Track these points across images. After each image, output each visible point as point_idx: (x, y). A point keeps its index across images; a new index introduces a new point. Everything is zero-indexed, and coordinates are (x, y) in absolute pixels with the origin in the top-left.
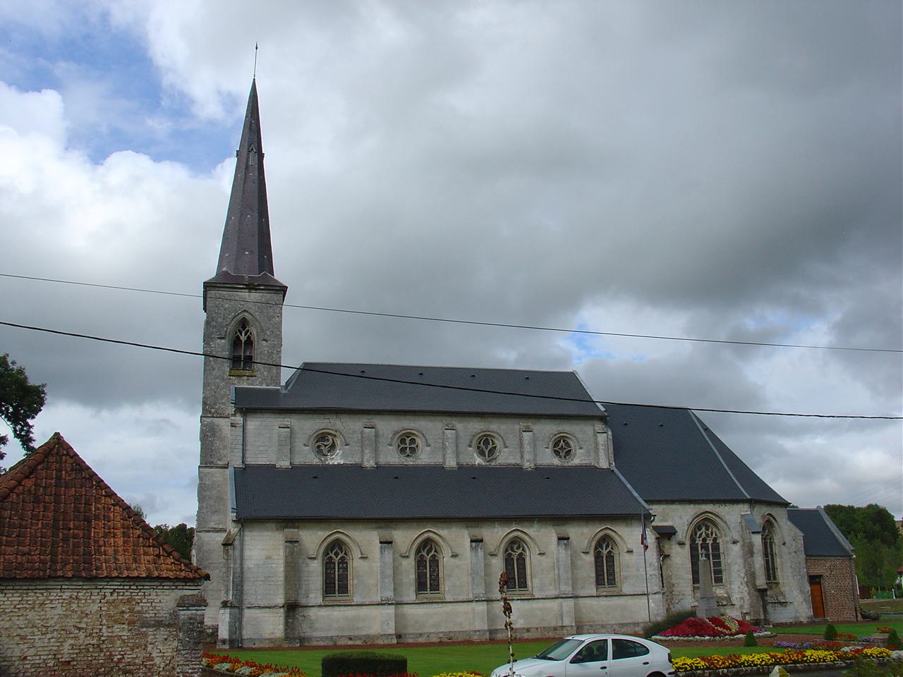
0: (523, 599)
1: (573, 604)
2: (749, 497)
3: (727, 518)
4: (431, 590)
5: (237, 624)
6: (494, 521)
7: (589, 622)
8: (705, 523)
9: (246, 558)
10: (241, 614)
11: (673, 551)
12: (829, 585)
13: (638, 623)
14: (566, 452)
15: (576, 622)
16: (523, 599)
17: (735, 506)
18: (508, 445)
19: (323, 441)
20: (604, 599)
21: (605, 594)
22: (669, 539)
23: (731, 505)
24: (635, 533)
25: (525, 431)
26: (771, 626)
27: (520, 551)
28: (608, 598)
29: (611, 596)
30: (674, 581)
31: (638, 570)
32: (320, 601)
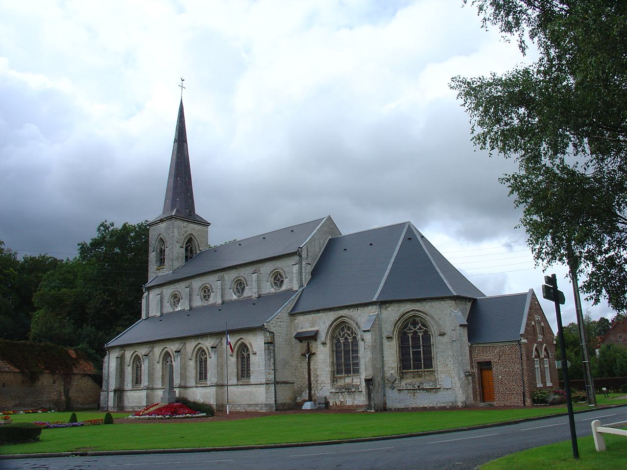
0: (203, 387)
1: (145, 393)
2: (455, 294)
3: (359, 320)
4: (424, 368)
5: (106, 400)
6: (256, 331)
7: (233, 402)
8: (340, 327)
9: (110, 367)
10: (108, 394)
11: (319, 349)
12: (498, 372)
13: (258, 404)
14: (240, 285)
15: (216, 402)
16: (203, 387)
17: (366, 308)
18: (248, 284)
19: (206, 292)
20: (241, 387)
21: (241, 383)
22: (316, 341)
23: (362, 308)
24: (259, 340)
25: (253, 273)
26: (373, 411)
27: (205, 356)
28: (243, 387)
29: (244, 385)
30: (318, 373)
31: (259, 366)
32: (235, 382)
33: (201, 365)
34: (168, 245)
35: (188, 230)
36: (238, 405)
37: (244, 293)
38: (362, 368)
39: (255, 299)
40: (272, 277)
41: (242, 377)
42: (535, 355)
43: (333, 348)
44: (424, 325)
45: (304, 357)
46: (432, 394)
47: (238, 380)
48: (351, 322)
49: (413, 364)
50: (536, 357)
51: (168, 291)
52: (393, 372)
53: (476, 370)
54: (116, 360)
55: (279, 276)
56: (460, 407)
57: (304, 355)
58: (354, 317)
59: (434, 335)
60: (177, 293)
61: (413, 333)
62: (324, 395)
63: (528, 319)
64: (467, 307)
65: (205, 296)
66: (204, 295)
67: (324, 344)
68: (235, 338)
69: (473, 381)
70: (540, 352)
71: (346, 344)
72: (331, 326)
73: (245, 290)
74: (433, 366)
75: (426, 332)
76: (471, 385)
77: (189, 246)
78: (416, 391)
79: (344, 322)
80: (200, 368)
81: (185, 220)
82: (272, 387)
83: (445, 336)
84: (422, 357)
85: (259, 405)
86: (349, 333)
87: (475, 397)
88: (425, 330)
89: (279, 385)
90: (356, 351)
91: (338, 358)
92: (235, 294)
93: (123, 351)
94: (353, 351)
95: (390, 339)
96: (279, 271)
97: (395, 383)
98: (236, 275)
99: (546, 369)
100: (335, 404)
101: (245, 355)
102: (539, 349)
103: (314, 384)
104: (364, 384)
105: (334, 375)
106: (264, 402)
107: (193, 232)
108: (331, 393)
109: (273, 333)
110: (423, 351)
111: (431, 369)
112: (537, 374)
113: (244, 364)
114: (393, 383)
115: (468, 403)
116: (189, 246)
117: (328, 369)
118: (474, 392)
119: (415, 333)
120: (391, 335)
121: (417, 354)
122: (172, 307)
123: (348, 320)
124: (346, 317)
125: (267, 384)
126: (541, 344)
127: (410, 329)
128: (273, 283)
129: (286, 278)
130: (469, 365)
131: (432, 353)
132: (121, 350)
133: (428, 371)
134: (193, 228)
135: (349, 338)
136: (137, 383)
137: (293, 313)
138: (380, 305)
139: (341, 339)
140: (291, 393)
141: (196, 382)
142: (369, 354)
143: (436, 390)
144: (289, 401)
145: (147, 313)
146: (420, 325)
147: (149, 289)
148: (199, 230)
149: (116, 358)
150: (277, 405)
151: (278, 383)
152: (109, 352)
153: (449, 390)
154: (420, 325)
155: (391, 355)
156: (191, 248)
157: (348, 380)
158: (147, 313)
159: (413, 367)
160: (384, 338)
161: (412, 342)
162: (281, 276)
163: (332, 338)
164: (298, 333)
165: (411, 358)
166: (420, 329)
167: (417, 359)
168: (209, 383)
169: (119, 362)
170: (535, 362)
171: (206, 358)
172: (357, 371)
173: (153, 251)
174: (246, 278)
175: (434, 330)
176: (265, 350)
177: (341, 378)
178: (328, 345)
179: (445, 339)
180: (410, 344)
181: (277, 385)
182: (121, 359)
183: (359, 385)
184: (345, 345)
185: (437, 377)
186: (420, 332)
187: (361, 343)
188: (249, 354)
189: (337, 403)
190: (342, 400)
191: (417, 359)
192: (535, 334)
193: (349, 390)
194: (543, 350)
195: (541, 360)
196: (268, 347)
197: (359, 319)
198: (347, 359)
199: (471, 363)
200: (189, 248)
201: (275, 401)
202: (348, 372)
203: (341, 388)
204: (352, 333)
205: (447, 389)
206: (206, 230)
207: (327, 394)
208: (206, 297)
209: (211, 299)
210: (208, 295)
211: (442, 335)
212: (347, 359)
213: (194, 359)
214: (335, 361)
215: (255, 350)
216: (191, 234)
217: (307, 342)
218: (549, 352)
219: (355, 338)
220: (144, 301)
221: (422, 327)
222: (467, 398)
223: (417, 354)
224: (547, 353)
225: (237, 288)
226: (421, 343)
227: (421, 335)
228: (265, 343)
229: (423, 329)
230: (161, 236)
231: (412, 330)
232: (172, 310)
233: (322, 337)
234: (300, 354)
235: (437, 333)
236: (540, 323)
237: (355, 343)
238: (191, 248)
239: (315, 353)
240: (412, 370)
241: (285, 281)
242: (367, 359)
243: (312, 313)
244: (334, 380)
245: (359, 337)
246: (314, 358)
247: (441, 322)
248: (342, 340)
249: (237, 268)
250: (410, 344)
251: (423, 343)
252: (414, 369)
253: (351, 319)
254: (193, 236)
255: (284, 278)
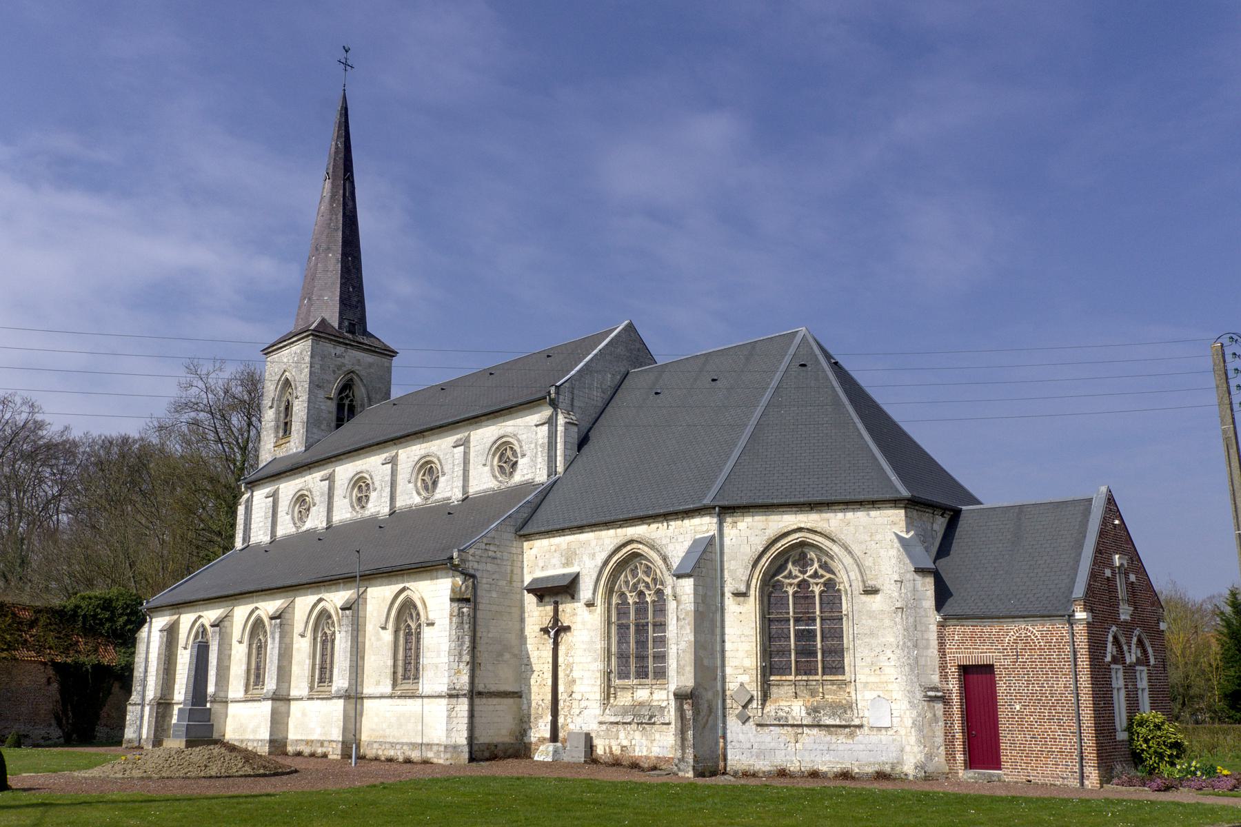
4: (824, 674)
13: (432, 745)
14: (429, 471)
19: (361, 486)
29: (405, 697)
31: (439, 656)
32: (387, 689)
33: (324, 649)
34: (299, 394)
35: (346, 362)
36: (391, 743)
37: (437, 491)
38: (672, 664)
39: (456, 503)
40: (494, 455)
41: (404, 679)
42: (1113, 657)
43: (609, 617)
44: (825, 566)
45: (546, 636)
46: (842, 739)
47: (394, 684)
48: (653, 555)
49: (796, 662)
50: (1115, 660)
51: (288, 489)
52: (745, 679)
53: (954, 686)
54: (160, 636)
55: (509, 453)
56: (911, 778)
57: (545, 631)
58: (658, 542)
59: (849, 592)
60: (306, 493)
61: (799, 585)
62: (586, 729)
63: (1095, 561)
64: (936, 527)
65: (359, 499)
66: (359, 495)
67: (590, 604)
68: (392, 587)
69: (948, 714)
70: (1125, 648)
71: (641, 608)
72: (606, 563)
73: (439, 485)
74: (846, 668)
75: (830, 585)
76: (941, 723)
77: (347, 396)
78: (800, 730)
79: (635, 555)
80: (323, 655)
81: (340, 342)
82: (463, 706)
83: (878, 597)
84: (819, 646)
85: (435, 748)
86: (648, 580)
87: (950, 756)
88: (830, 579)
89: (484, 700)
90: (661, 626)
91: (623, 639)
92: (419, 494)
93: (178, 616)
94: (655, 625)
95: (742, 599)
96: (510, 440)
97: (749, 707)
98: (423, 452)
99: (1140, 692)
100: (608, 751)
101: (413, 626)
102: (1123, 640)
103: (565, 701)
104: (672, 703)
105: (609, 680)
106: (444, 740)
107: (357, 367)
108: (601, 723)
109: (473, 576)
110: (822, 628)
111: (840, 677)
112: (1116, 706)
113: (411, 649)
114: (745, 707)
115: (930, 768)
116: (347, 396)
117: (598, 666)
118: (949, 742)
119: (803, 584)
120: (743, 589)
121: (806, 636)
122: (295, 524)
123: (646, 549)
124: (640, 543)
125: (450, 696)
126: (1127, 628)
127: (790, 576)
128: (496, 468)
129: (523, 456)
130: (938, 671)
131: (845, 638)
132: (173, 615)
133: (833, 682)
134: (353, 358)
135: (647, 592)
136: (256, 684)
137: (278, 444)
138: (719, 515)
139: (628, 594)
140: (514, 718)
141: (311, 688)
142: (689, 631)
143: (851, 728)
144: (507, 740)
145: (246, 537)
146: (816, 565)
147: (253, 485)
148: (370, 365)
149: (160, 631)
150: (475, 748)
151: (480, 694)
152: (151, 618)
153: (883, 732)
154: (816, 565)
155: (743, 639)
156: (352, 401)
157: (642, 694)
158: (246, 537)
159: (797, 669)
160: (728, 595)
161: (794, 608)
162: (514, 453)
163: (610, 592)
164: (535, 581)
165: (793, 647)
166: (815, 575)
167: (806, 652)
168: (334, 689)
169: (165, 639)
170: (1113, 674)
171: (334, 632)
172: (661, 674)
173: (271, 407)
174: (441, 457)
175: (847, 577)
176: (451, 615)
177: (624, 688)
178: (599, 608)
179: (875, 602)
180: (791, 614)
181: (477, 701)
182: (171, 632)
183: (665, 707)
184: (637, 611)
185: (854, 697)
186: (817, 584)
187: (671, 605)
188: (420, 625)
189: (614, 749)
190: (625, 743)
191: (806, 652)
192: (1113, 604)
193: (645, 718)
194: (1133, 647)
195: (1130, 671)
196: (459, 609)
197: (671, 547)
198: (641, 644)
199: (943, 667)
200: (347, 402)
201: (471, 738)
202: (642, 673)
203: (625, 711)
204: (655, 580)
205: (879, 729)
206: (386, 364)
207: (591, 726)
208: (362, 501)
209: (370, 505)
210: (366, 496)
211: (871, 591)
212: (641, 644)
213: (309, 634)
214: (614, 649)
215: (431, 616)
216: (353, 372)
217: (552, 600)
218: (1150, 650)
219: (659, 593)
220: (241, 510)
221: (821, 572)
222: (929, 757)
223: (806, 636)
224: (1145, 652)
225: (423, 480)
226: (818, 613)
227: (817, 590)
228: (452, 600)
229: (822, 576)
230: (287, 373)
231: (796, 577)
232: (294, 529)
233: (585, 591)
234: (537, 628)
235: (858, 586)
236: (1127, 574)
237: (660, 607)
238: (352, 401)
239: (568, 629)
240: (792, 678)
241: (522, 462)
242: (683, 645)
243: (567, 532)
244: (608, 694)
245: (668, 591)
246: (565, 639)
247: (868, 562)
248: (631, 598)
249: (424, 437)
250: (791, 614)
251: (821, 612)
252: (796, 675)
253: (652, 547)
254: (357, 375)
255: (519, 455)
